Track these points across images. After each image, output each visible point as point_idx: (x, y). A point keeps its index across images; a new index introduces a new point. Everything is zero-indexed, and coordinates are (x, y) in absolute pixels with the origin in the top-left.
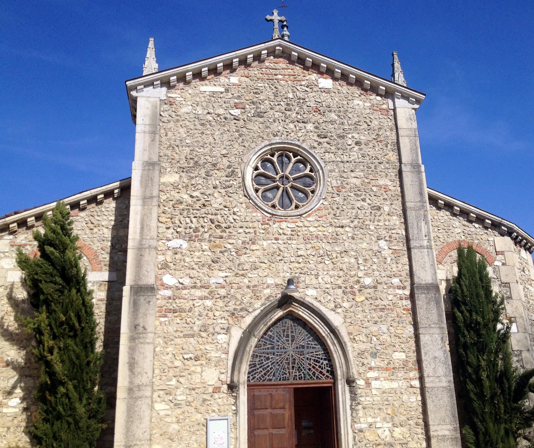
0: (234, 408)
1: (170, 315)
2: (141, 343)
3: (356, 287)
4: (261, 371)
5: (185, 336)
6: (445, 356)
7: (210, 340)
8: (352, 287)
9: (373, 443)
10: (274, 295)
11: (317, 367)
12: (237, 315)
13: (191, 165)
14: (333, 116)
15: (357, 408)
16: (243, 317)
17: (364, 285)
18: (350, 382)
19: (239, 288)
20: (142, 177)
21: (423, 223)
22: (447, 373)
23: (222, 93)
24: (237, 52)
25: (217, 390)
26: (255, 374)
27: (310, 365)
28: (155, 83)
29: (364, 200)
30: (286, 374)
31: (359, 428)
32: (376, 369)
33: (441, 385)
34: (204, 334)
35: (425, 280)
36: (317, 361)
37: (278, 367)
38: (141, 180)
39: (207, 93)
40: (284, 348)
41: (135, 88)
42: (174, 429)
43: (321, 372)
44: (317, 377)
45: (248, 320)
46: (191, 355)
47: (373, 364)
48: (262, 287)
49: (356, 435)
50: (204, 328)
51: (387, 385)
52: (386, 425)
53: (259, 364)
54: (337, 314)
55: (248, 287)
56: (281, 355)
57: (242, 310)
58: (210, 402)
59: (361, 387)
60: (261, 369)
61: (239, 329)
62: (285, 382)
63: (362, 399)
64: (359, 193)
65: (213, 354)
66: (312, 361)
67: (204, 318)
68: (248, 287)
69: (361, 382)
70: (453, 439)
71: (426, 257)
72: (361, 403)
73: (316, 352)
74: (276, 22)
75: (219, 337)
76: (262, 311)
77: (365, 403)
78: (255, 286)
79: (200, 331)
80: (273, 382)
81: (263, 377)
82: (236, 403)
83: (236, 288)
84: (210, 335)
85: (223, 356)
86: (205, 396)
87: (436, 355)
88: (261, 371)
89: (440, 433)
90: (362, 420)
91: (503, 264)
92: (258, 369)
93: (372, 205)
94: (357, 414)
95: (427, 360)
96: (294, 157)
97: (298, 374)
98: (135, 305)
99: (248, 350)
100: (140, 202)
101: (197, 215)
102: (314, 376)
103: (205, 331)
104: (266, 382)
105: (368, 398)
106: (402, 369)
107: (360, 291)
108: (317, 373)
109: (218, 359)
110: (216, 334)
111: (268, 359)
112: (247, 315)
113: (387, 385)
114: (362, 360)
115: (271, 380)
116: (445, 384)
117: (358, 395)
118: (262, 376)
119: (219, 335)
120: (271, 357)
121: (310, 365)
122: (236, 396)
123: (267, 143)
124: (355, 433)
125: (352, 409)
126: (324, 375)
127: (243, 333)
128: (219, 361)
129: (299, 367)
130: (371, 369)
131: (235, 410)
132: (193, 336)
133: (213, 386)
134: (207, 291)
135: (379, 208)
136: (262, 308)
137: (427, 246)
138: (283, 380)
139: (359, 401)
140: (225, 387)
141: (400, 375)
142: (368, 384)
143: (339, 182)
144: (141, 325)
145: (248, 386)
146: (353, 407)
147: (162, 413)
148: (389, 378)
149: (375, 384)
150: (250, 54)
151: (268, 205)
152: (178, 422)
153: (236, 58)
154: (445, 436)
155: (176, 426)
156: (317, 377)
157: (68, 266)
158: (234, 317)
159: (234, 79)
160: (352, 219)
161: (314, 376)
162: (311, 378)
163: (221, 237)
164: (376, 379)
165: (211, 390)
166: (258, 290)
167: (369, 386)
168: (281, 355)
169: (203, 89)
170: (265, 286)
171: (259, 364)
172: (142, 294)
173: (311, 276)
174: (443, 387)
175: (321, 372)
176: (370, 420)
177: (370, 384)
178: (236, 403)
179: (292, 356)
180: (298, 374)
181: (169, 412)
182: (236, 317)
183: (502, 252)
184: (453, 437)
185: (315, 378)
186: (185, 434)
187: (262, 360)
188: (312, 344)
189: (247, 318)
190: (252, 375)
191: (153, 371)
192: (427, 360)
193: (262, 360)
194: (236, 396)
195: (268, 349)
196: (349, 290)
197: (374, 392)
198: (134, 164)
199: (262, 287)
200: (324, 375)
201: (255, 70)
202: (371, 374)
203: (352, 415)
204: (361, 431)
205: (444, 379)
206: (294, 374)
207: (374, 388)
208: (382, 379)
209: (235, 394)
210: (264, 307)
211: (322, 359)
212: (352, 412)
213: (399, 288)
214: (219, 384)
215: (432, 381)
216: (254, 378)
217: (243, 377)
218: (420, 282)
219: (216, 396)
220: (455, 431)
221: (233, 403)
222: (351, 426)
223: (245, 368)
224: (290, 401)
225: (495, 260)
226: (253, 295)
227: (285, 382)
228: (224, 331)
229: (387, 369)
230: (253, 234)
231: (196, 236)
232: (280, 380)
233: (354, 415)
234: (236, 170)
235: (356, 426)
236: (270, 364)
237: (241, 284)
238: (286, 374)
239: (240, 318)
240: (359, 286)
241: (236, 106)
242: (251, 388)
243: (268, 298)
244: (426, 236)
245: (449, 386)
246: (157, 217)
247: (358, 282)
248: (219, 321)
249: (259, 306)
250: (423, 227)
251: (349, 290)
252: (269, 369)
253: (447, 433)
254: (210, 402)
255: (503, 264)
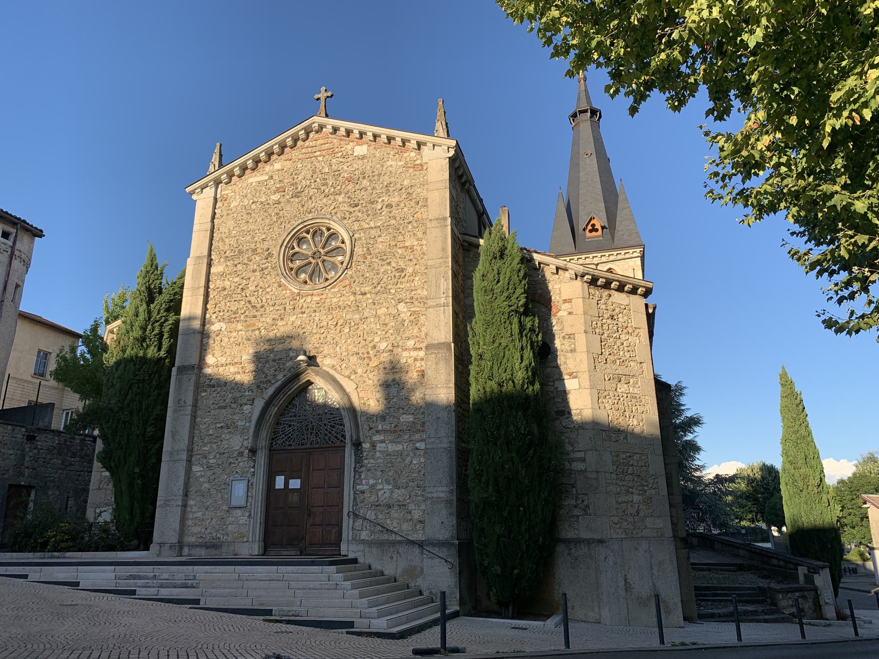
1: (208, 390)
2: (182, 415)
4: (283, 438)
5: (219, 408)
6: (449, 416)
8: (368, 353)
11: (333, 432)
13: (236, 253)
14: (365, 183)
18: (357, 445)
20: (193, 271)
21: (442, 280)
22: (449, 434)
23: (266, 181)
24: (275, 139)
25: (241, 454)
26: (278, 440)
27: (327, 430)
28: (209, 184)
29: (389, 264)
30: (304, 440)
32: (384, 432)
33: (442, 446)
34: (234, 406)
35: (438, 340)
36: (333, 427)
37: (298, 433)
38: (193, 274)
39: (253, 184)
40: (305, 416)
41: (193, 192)
42: (205, 488)
43: (336, 437)
44: (332, 442)
45: (271, 391)
46: (222, 424)
47: (380, 428)
50: (235, 400)
51: (391, 448)
52: (386, 487)
53: (282, 431)
55: (274, 361)
56: (301, 422)
59: (367, 450)
60: (283, 436)
62: (303, 447)
63: (366, 461)
64: (385, 257)
66: (329, 427)
68: (274, 361)
69: (366, 446)
70: (448, 502)
71: (442, 315)
73: (333, 418)
74: (319, 96)
77: (369, 465)
78: (280, 359)
79: (231, 403)
80: (292, 447)
81: (285, 443)
85: (247, 424)
86: (231, 460)
87: (440, 415)
88: (283, 438)
89: (435, 495)
90: (364, 482)
91: (570, 313)
92: (281, 435)
93: (396, 268)
95: (429, 421)
96: (308, 234)
97: (315, 439)
98: (179, 381)
99: (268, 418)
100: (190, 293)
101: (237, 299)
102: (330, 440)
103: (235, 402)
104: (287, 447)
106: (408, 431)
108: (332, 438)
111: (290, 426)
113: (391, 448)
115: (291, 445)
116: (445, 445)
118: (283, 441)
120: (292, 424)
121: (327, 430)
123: (300, 221)
125: (355, 471)
126: (338, 439)
129: (317, 433)
130: (378, 432)
132: (225, 407)
133: (238, 451)
135: (402, 270)
136: (283, 380)
137: (444, 303)
138: (302, 445)
141: (406, 437)
142: (373, 446)
143: (365, 249)
144: (183, 400)
147: (199, 474)
148: (395, 440)
149: (380, 447)
150: (288, 137)
151: (566, 260)
152: (209, 482)
153: (276, 144)
154: (440, 498)
155: (207, 485)
156: (332, 442)
159: (277, 166)
160: (375, 285)
161: (330, 440)
162: (327, 442)
163: (255, 317)
164: (382, 442)
168: (301, 422)
169: (250, 181)
170: (288, 359)
171: (282, 431)
172: (185, 373)
174: (444, 448)
175: (336, 437)
176: (371, 482)
177: (376, 446)
179: (312, 423)
180: (315, 439)
181: (203, 474)
183: (570, 299)
184: (448, 499)
185: (330, 443)
186: (213, 491)
187: (285, 427)
190: (275, 441)
191: (193, 438)
192: (429, 421)
193: (285, 427)
195: (291, 416)
196: (366, 355)
197: (378, 454)
198: (189, 260)
200: (338, 439)
201: (295, 154)
202: (377, 438)
204: (363, 492)
205: (445, 440)
206: (311, 439)
208: (387, 442)
211: (338, 424)
213: (415, 349)
215: (432, 442)
216: (276, 444)
217: (263, 442)
218: (433, 342)
220: (451, 493)
223: (264, 434)
225: (560, 310)
227: (303, 447)
228: (250, 402)
229: (395, 432)
230: (283, 311)
231: (235, 318)
232: (299, 445)
233: (357, 477)
234: (272, 252)
236: (291, 430)
238: (304, 440)
241: (278, 190)
244: (443, 293)
245: (449, 447)
246: (562, 293)
247: (374, 347)
250: (442, 284)
252: (290, 435)
253: (442, 495)
255: (570, 313)
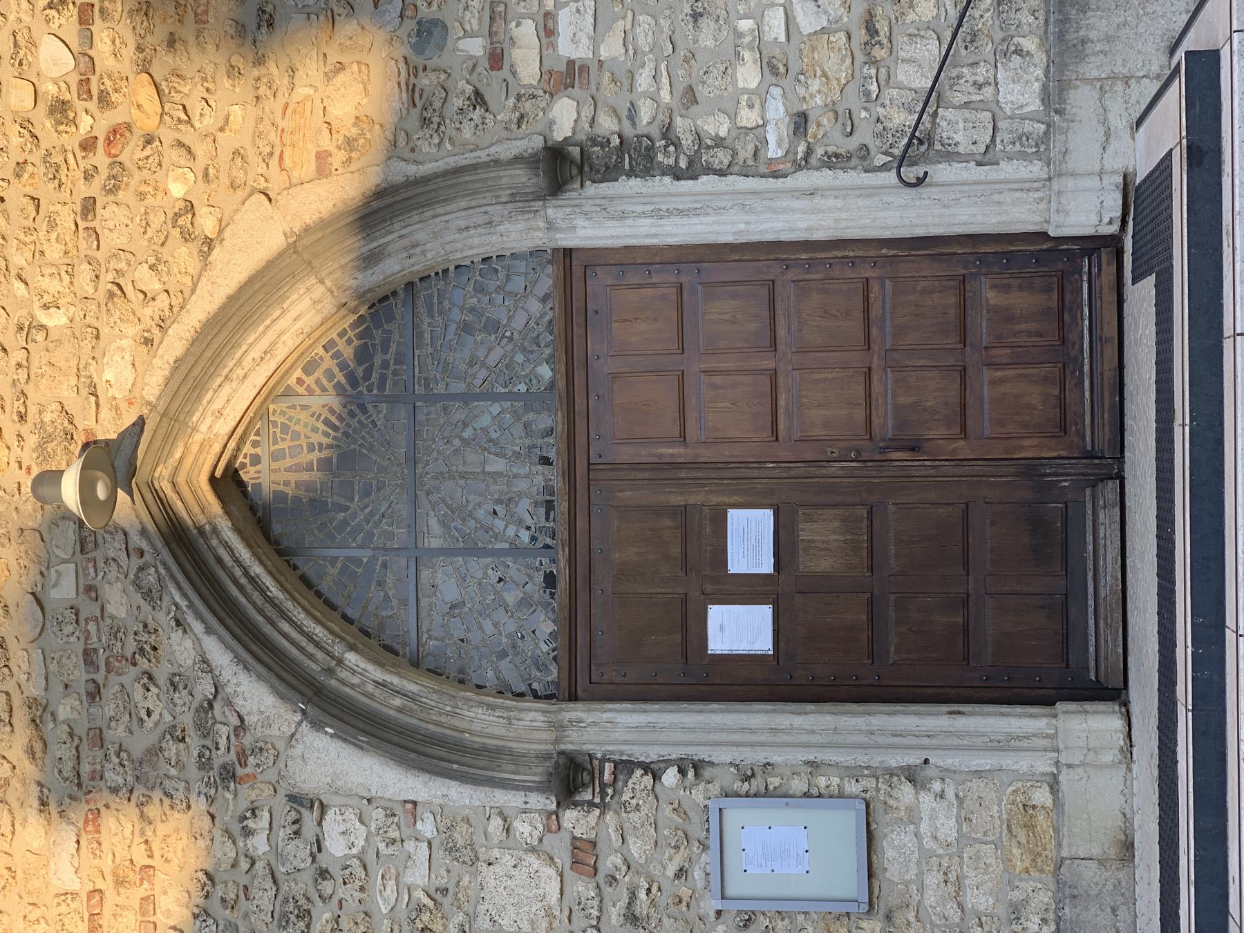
0: (670, 777)
3: (85, 122)
7: (349, 893)
9: (860, 58)
10: (136, 562)
12: (233, 756)
15: (687, 141)
16: (241, 726)
17: (74, 80)
19: (99, 738)
31: (785, 130)
47: (476, 47)
48: (92, 627)
49: (820, 151)
54: (227, 234)
55: (94, 693)
57: (205, 730)
58: (642, 895)
59: (587, 112)
61: (299, 749)
63: (645, 114)
65: (417, 876)
67: (246, 915)
68: (94, 693)
72: (663, 117)
75: (336, 847)
76: (209, 631)
77: (665, 95)
78: (89, 656)
82: (647, 768)
83: (100, 754)
84: (327, 887)
85: (427, 827)
90: (748, 117)
94: (719, 142)
105: (644, 80)
107: (104, 100)
109: (439, 853)
110: (323, 861)
112: (230, 703)
114: (457, 102)
117: (628, 131)
119: (327, 843)
122: (616, 764)
124: (807, 157)
127: (317, 726)
128: (451, 849)
130: (496, 59)
131: (682, 772)
134: (111, 897)
136: (198, 627)
139: (655, 131)
140: (570, 816)
145: (573, 697)
146: (683, 164)
157: (188, 31)
158: (240, 771)
164: (548, 31)
165: (582, 888)
166: (109, 647)
167: (584, 68)
170: (89, 609)
173: (35, 363)
176: (749, 75)
177: (571, 63)
178: (647, 768)
182: (242, 759)
188: (385, 365)
189: (242, 705)
194: (616, 764)
197: (611, 49)
199: (92, 627)
203: (721, 173)
204: (801, 122)
207: (595, 42)
209: (608, 767)
210: (190, 618)
212: (709, 170)
214: (560, 847)
219: (610, 861)
221: (648, 779)
222: (776, 175)
224: (791, 230)
226: (133, 672)
228: (309, 819)
233: (721, 158)
235: (774, 151)
237: (81, 730)
239: (247, 740)
240: (79, 105)
242: (582, 682)
243: (147, 594)
247: (60, 110)
248: (259, 845)
249: (188, 643)
251: (100, 158)
254: (642, 895)
